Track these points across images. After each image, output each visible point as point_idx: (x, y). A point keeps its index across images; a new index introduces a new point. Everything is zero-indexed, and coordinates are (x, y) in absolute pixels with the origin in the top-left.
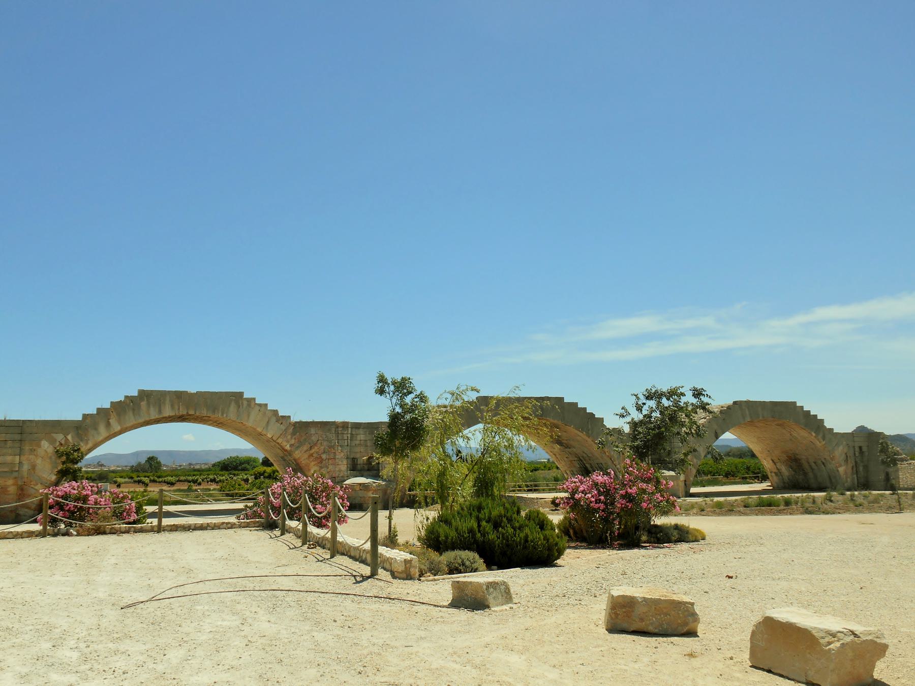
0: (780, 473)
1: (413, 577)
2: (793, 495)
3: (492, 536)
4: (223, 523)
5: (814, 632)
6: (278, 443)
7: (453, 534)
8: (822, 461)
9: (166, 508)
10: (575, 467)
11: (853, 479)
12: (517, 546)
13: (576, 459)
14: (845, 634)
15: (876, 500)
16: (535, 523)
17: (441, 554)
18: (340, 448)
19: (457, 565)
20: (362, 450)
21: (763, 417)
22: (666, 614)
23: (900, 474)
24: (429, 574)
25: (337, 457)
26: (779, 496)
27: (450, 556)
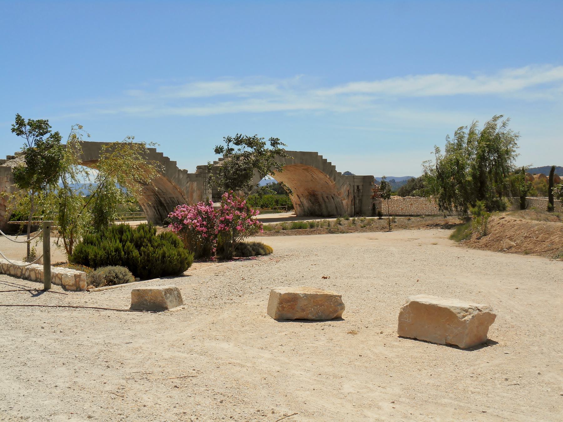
0: (302, 205)
2: (314, 220)
3: (136, 253)
5: (452, 309)
7: (101, 253)
8: (332, 196)
11: (352, 209)
12: (156, 261)
13: (152, 194)
14: (473, 310)
15: (369, 224)
16: (169, 242)
17: (95, 270)
19: (112, 278)
21: (295, 163)
22: (321, 305)
23: (382, 205)
24: (92, 286)
26: (305, 221)
27: (102, 272)
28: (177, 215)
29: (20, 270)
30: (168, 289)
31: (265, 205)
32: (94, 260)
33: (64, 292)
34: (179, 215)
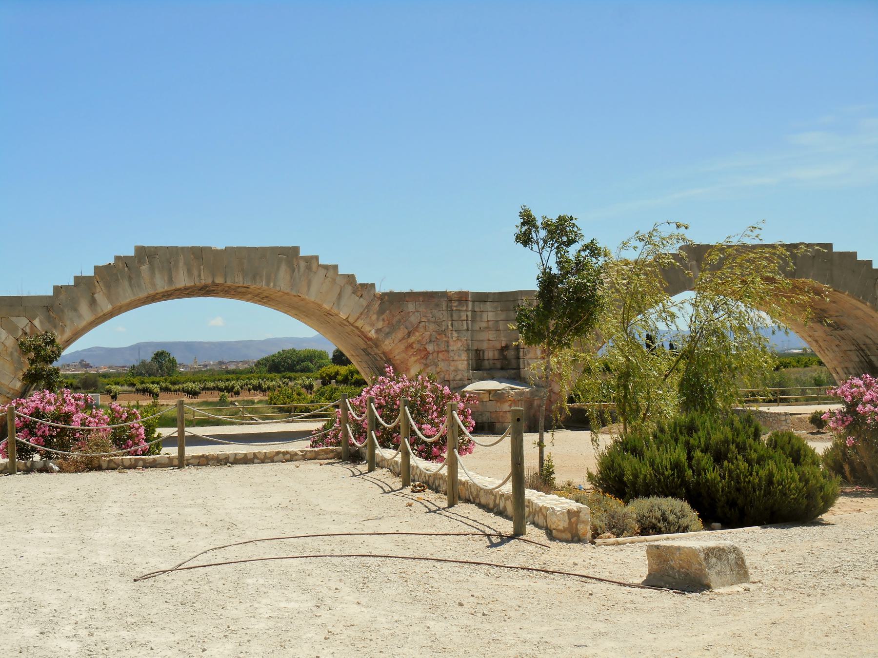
1: (582, 537)
3: (712, 475)
4: (278, 453)
6: (357, 328)
7: (646, 470)
9: (190, 431)
10: (851, 361)
13: (853, 348)
18: (455, 334)
19: (654, 520)
20: (491, 337)
25: (451, 348)
28: (843, 392)
29: (493, 497)
30: (714, 549)
32: (634, 484)
33: (547, 542)
34: (848, 393)
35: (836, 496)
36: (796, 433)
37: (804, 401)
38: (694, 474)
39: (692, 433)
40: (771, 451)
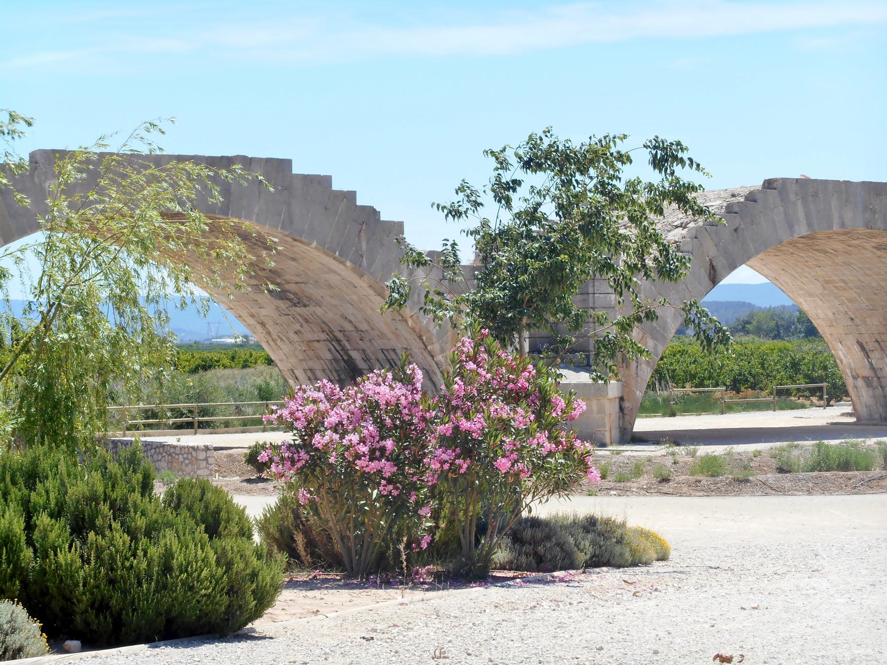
10: (319, 358)
13: (323, 336)
21: (843, 225)
26: (872, 441)
28: (292, 414)
31: (746, 381)
35: (276, 589)
36: (217, 481)
37: (240, 425)
38: (36, 557)
39: (34, 484)
40: (170, 515)
